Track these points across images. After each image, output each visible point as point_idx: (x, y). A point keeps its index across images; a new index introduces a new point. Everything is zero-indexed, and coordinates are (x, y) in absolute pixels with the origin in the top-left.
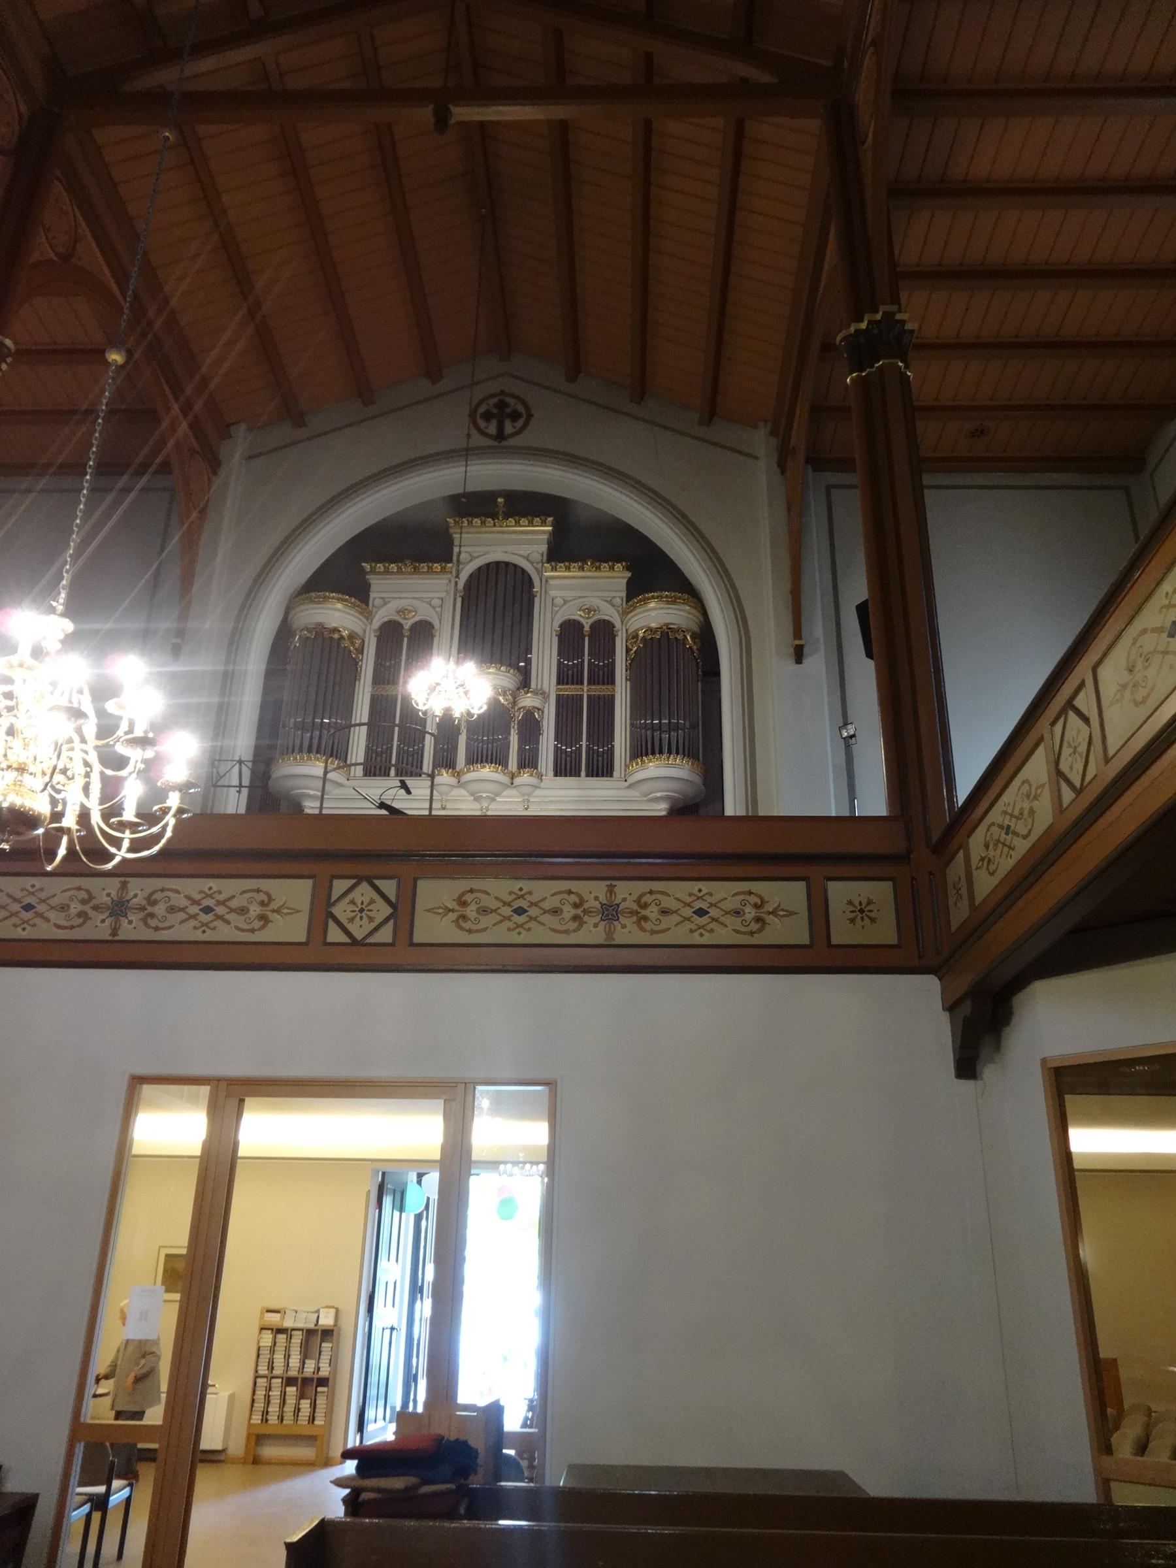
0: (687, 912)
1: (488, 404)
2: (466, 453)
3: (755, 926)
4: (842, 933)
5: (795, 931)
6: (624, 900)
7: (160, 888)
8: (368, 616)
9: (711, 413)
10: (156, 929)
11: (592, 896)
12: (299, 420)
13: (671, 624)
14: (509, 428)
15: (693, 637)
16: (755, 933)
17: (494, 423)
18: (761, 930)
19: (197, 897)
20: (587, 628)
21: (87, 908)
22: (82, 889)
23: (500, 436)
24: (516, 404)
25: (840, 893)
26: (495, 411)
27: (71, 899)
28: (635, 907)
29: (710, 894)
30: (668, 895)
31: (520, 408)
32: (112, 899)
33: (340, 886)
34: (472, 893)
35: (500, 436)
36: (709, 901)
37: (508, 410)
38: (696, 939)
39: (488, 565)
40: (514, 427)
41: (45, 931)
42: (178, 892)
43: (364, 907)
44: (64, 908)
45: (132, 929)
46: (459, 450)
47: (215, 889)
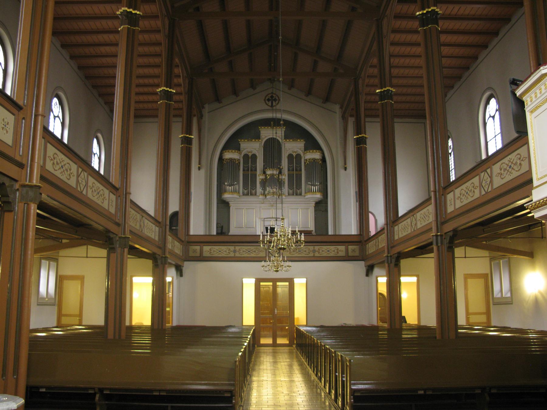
0: (326, 251)
3: (337, 253)
4: (350, 254)
5: (342, 254)
8: (240, 154)
9: (327, 100)
10: (241, 255)
14: (274, 104)
15: (321, 161)
20: (294, 156)
21: (229, 251)
23: (272, 106)
25: (351, 247)
26: (270, 98)
28: (318, 250)
31: (277, 98)
37: (274, 98)
38: (328, 255)
39: (269, 139)
41: (223, 255)
42: (244, 248)
44: (226, 251)
45: (237, 255)
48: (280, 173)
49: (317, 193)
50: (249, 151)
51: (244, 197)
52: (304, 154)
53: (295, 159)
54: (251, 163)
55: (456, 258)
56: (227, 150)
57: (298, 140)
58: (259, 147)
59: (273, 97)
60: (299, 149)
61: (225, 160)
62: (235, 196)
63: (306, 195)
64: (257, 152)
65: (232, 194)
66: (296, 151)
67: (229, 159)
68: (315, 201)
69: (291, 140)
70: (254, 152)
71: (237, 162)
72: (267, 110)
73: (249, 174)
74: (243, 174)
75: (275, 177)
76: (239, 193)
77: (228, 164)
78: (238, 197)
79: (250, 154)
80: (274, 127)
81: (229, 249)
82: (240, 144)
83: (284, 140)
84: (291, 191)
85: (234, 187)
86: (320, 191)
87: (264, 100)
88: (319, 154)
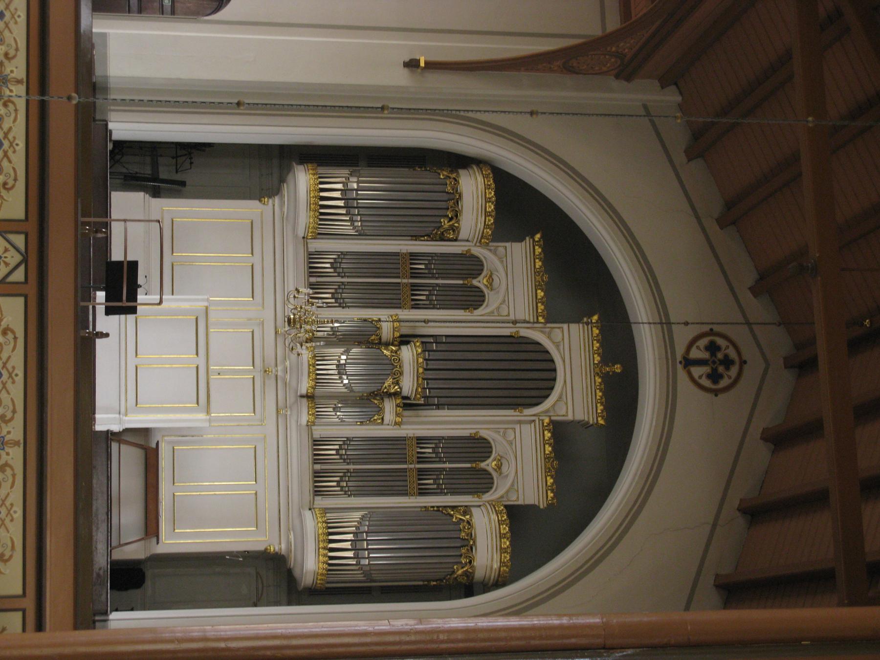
1: (728, 347)
2: (665, 323)
6: (8, 454)
7: (18, 108)
8: (482, 240)
11: (10, 429)
12: (691, 154)
13: (476, 549)
14: (697, 371)
15: (466, 574)
16: (14, 473)
17: (705, 355)
18: (13, 332)
19: (10, 137)
20: (483, 465)
22: (17, 52)
24: (729, 377)
26: (720, 356)
27: (9, 45)
29: (12, 520)
30: (12, 487)
32: (9, 75)
33: (19, 240)
34: (14, 339)
35: (688, 363)
36: (6, 519)
37: (721, 369)
40: (700, 377)
42: (15, 120)
43: (3, 259)
46: (667, 315)
47: (17, 148)
48: (408, 405)
49: (325, 555)
50: (494, 277)
51: (307, 444)
52: (493, 504)
53: (468, 465)
54: (444, 285)
55: (574, 418)
56: (495, 181)
57: (552, 477)
58: (512, 317)
59: (728, 368)
60: (512, 485)
61: (454, 175)
62: (304, 219)
63: (315, 517)
64: (488, 310)
65: (309, 204)
66: (505, 468)
67: (455, 189)
68: (289, 549)
69: (548, 449)
70: (493, 301)
71: (446, 223)
72: (668, 341)
73: (399, 277)
74: (396, 254)
75: (389, 381)
76: (318, 235)
77: (437, 188)
78: (301, 233)
79: (480, 282)
80: (602, 378)
81: (14, 57)
82: (521, 239)
83: (547, 420)
84: (331, 450)
85: (343, 211)
86: (332, 567)
87: (716, 395)
88: (496, 566)
